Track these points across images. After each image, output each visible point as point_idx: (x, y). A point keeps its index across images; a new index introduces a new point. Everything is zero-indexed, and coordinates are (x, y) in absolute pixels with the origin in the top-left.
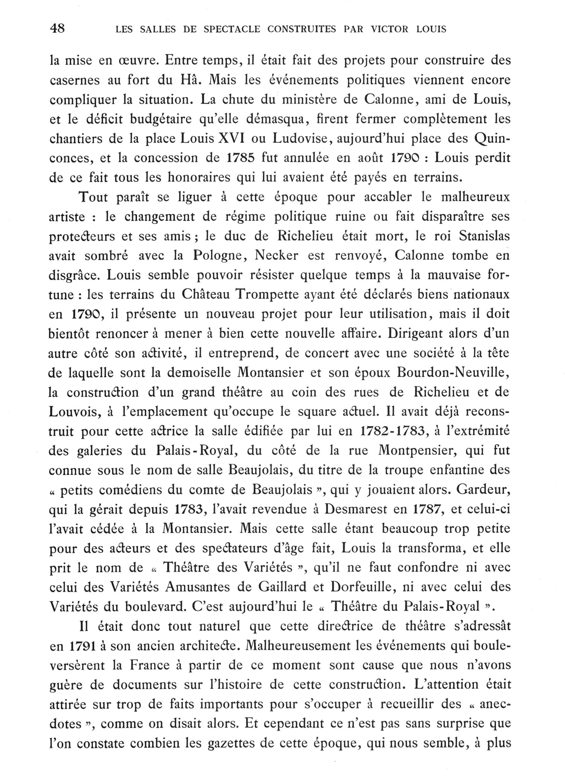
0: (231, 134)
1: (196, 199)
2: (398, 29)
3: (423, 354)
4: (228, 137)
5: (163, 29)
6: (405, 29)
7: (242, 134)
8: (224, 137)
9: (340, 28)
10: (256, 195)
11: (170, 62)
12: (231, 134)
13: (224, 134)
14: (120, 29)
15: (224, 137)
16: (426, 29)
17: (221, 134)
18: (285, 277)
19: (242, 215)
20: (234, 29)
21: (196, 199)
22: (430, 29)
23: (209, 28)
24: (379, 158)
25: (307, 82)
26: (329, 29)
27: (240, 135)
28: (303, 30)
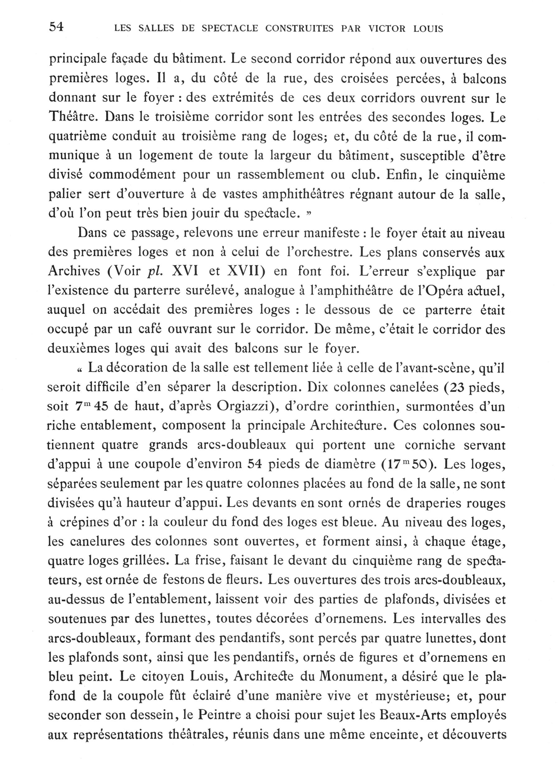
0: (185, 266)
1: (285, 292)
2: (395, 28)
3: (198, 426)
4: (182, 270)
5: (162, 28)
6: (402, 29)
7: (196, 266)
8: (177, 270)
9: (337, 28)
10: (457, 637)
11: (391, 176)
12: (185, 266)
13: (178, 267)
14: (119, 27)
15: (177, 270)
16: (423, 29)
17: (175, 266)
18: (85, 292)
19: (240, 405)
20: (232, 28)
21: (285, 292)
22: (427, 28)
23: (207, 27)
24: (181, 696)
25: (299, 177)
26: (326, 28)
27: (193, 267)
28: (301, 29)
